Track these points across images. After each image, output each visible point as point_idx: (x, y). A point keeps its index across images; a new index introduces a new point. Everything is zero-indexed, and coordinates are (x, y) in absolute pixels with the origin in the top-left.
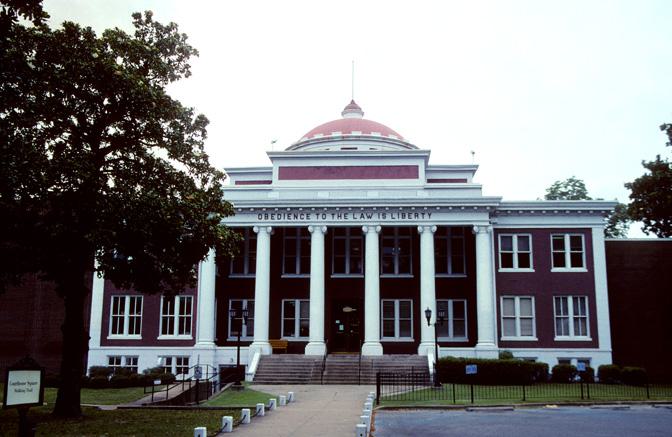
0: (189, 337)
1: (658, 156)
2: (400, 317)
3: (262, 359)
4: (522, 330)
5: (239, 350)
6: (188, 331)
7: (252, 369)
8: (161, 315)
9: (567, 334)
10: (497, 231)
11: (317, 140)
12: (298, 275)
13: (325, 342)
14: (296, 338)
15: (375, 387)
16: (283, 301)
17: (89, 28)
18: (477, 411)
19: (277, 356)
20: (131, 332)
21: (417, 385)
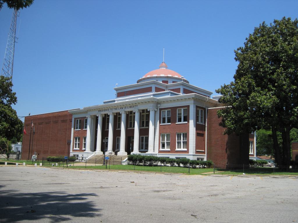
8: (83, 143)
20: (183, 148)
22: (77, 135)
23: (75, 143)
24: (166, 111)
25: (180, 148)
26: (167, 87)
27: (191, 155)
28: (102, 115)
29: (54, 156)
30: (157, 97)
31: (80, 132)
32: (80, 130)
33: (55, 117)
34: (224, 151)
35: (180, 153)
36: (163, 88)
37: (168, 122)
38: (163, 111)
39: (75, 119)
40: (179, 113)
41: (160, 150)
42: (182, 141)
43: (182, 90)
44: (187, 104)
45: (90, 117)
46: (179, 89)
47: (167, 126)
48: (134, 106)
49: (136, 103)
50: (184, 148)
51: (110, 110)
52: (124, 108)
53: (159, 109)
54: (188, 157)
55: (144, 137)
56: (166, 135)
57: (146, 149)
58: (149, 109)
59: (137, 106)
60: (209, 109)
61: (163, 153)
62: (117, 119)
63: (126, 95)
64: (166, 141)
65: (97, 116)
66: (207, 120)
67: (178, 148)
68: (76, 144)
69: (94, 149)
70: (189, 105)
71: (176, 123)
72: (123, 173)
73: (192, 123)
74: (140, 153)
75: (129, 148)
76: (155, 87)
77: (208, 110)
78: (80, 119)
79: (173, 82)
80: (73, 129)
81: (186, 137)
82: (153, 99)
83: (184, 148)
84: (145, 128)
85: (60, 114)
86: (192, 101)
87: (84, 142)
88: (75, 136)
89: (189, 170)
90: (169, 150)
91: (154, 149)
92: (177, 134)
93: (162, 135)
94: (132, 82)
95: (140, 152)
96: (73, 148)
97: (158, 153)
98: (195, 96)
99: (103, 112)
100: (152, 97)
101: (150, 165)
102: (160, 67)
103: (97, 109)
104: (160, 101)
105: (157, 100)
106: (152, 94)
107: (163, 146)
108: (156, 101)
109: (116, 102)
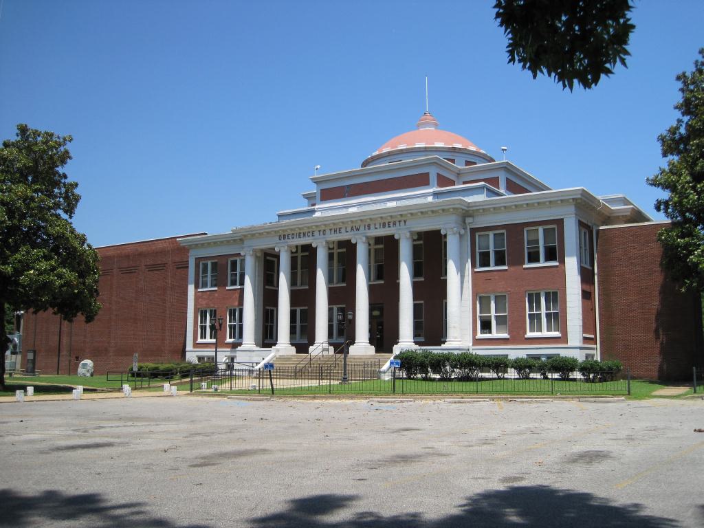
8: (228, 323)
9: (540, 330)
11: (402, 150)
15: (269, 380)
16: (422, 302)
17: (633, 27)
18: (233, 398)
20: (211, 338)
21: (322, 379)
22: (206, 304)
23: (199, 324)
24: (491, 234)
25: (540, 330)
26: (458, 174)
27: (575, 346)
28: (290, 247)
29: (148, 361)
30: (464, 197)
31: (216, 295)
32: (216, 289)
33: (128, 256)
34: (651, 336)
35: (540, 343)
36: (452, 178)
37: (548, 259)
39: (198, 260)
40: (531, 238)
41: (477, 337)
42: (543, 311)
43: (502, 183)
44: (557, 216)
45: (287, 251)
46: (497, 178)
47: (495, 273)
49: (401, 215)
50: (549, 329)
51: (316, 234)
52: (362, 228)
53: (470, 229)
54: (564, 353)
58: (446, 229)
59: (405, 222)
60: (601, 228)
61: (488, 344)
62: (304, 260)
63: (348, 196)
64: (493, 313)
66: (596, 256)
68: (203, 328)
69: (267, 337)
70: (562, 220)
71: (524, 266)
72: (388, 402)
73: (572, 265)
74: (417, 347)
75: (383, 336)
76: (438, 174)
77: (598, 231)
78: (213, 261)
79: (468, 163)
80: (191, 288)
81: (555, 301)
82: (459, 204)
83: (549, 329)
84: (335, 286)
85: (144, 249)
86: (572, 209)
87: (201, 323)
88: (199, 307)
89: (629, 385)
90: (506, 336)
91: (460, 335)
92: (478, 299)
93: (481, 299)
94: (348, 164)
95: (416, 343)
96: (195, 338)
97: (471, 344)
98: (582, 195)
100: (430, 199)
101: (466, 379)
102: (418, 127)
103: (275, 232)
104: (475, 208)
105: (466, 204)
106: (431, 190)
107: (486, 326)
108: (463, 210)
109: (318, 214)
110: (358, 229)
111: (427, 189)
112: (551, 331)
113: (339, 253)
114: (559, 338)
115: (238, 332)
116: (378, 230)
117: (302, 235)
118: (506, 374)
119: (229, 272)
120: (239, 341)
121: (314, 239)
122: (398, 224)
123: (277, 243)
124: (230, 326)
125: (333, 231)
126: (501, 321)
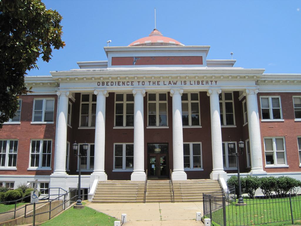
0: (49, 169)
1: (63, 48)
2: (194, 154)
3: (99, 184)
4: (115, 166)
5: (80, 178)
6: (48, 165)
7: (92, 192)
8: (31, 153)
10: (259, 94)
12: (124, 127)
13: (145, 171)
14: (124, 169)
16: (200, 143)
19: (111, 182)
20: (10, 165)
24: (270, 98)
31: (19, 128)
38: (278, 98)
48: (207, 82)
51: (136, 84)
52: (179, 83)
55: (124, 145)
56: (274, 140)
57: (90, 168)
59: (216, 82)
64: (275, 150)
65: (95, 93)
67: (32, 165)
71: (32, 123)
92: (264, 140)
99: (114, 86)
110: (175, 84)
111: (202, 67)
112: (34, 166)
113: (127, 104)
114: (16, 171)
115: (49, 160)
116: (193, 86)
117: (121, 84)
118: (75, 186)
119: (34, 110)
120: (128, 170)
121: (134, 87)
122: (210, 83)
123: (95, 88)
124: (33, 156)
125: (151, 83)
126: (280, 155)
